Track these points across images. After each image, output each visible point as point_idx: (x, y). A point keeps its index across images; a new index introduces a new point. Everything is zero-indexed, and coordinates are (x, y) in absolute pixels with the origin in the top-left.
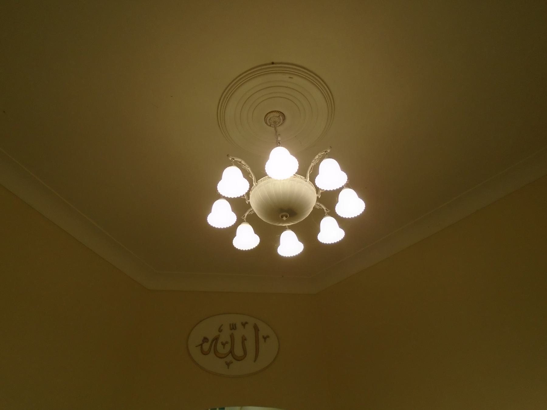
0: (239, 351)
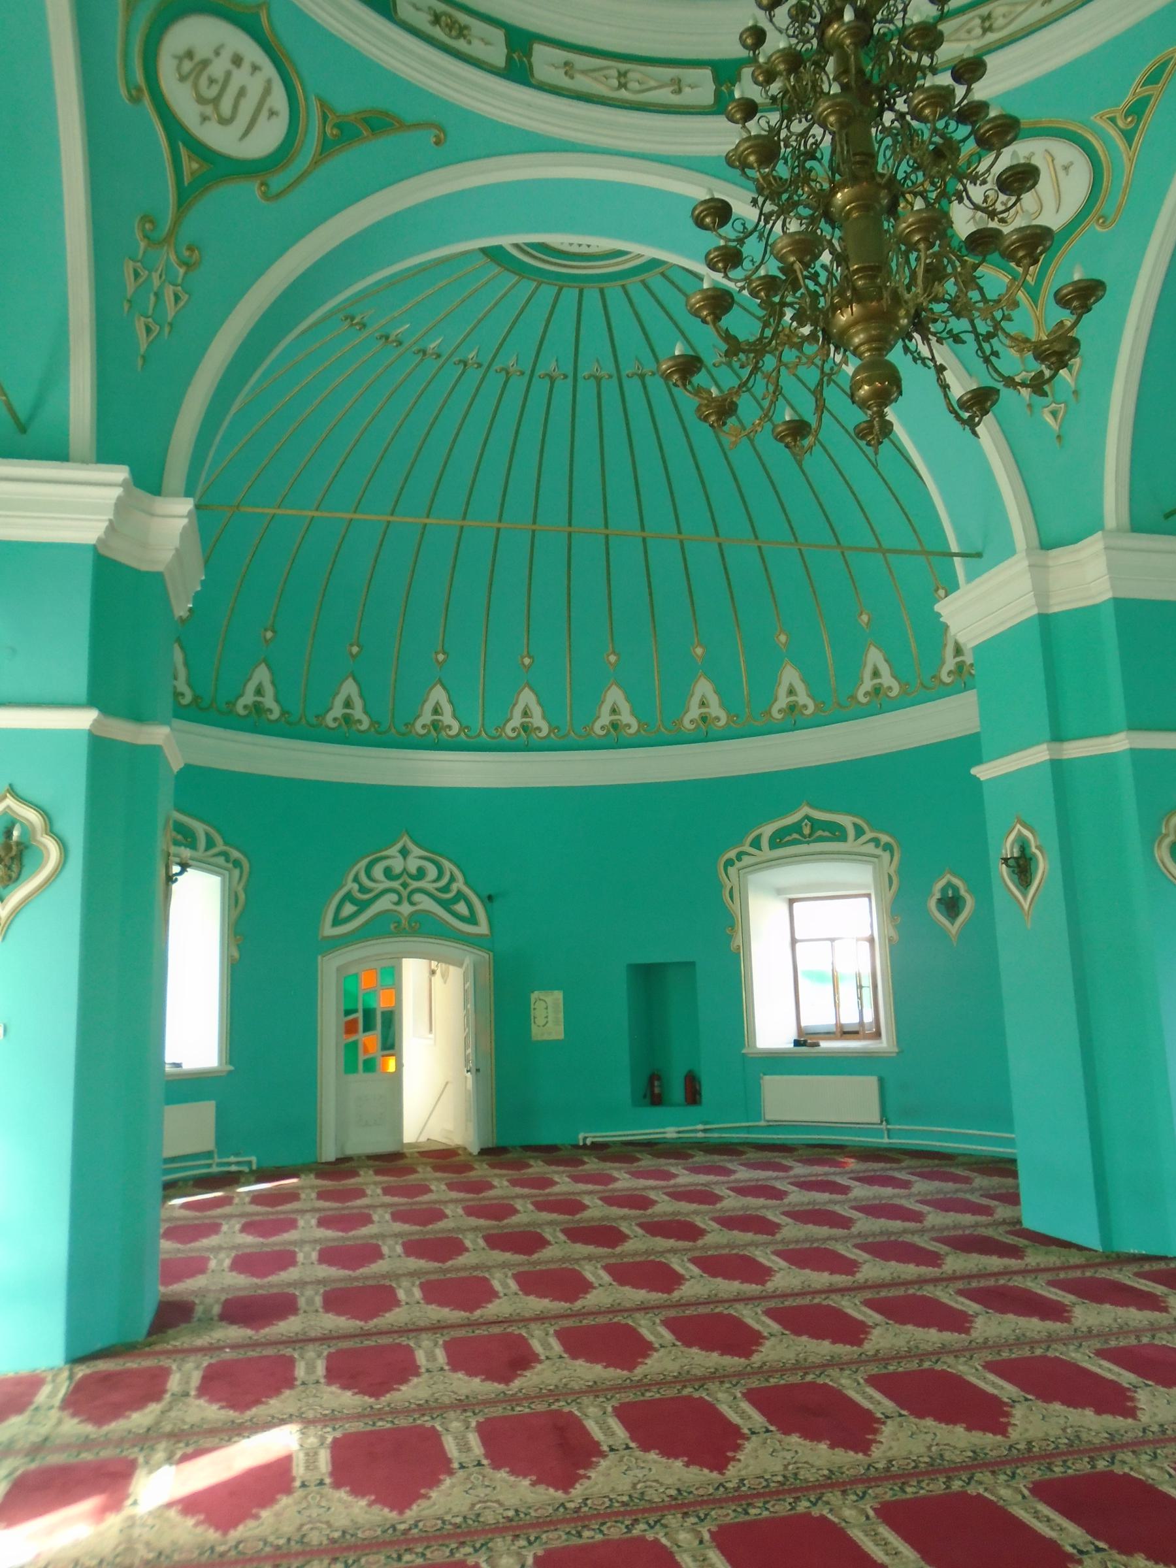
0: (226, 107)
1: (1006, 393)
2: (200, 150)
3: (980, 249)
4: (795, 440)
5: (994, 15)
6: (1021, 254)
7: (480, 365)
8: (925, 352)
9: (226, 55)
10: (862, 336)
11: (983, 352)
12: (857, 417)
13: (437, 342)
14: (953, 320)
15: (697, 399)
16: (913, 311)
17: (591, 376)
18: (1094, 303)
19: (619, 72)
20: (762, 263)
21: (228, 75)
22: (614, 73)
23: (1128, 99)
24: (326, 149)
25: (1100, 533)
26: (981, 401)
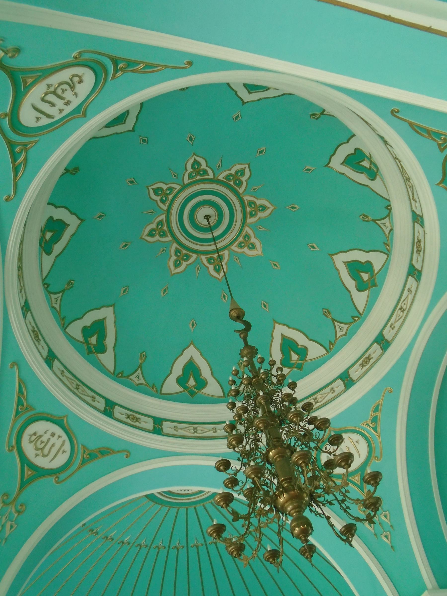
0: (46, 451)
1: (359, 525)
2: (33, 467)
3: (330, 467)
4: (274, 560)
5: (317, 398)
6: (343, 464)
7: (147, 546)
8: (320, 511)
9: (49, 433)
10: (291, 507)
11: (343, 508)
12: (299, 544)
13: (128, 538)
14: (326, 495)
15: (225, 544)
16: (309, 494)
17: (194, 545)
18: (380, 480)
19: (194, 428)
20: (246, 483)
21: (49, 439)
22: (192, 428)
23: (370, 417)
24: (84, 463)
25: (426, 591)
26: (349, 531)
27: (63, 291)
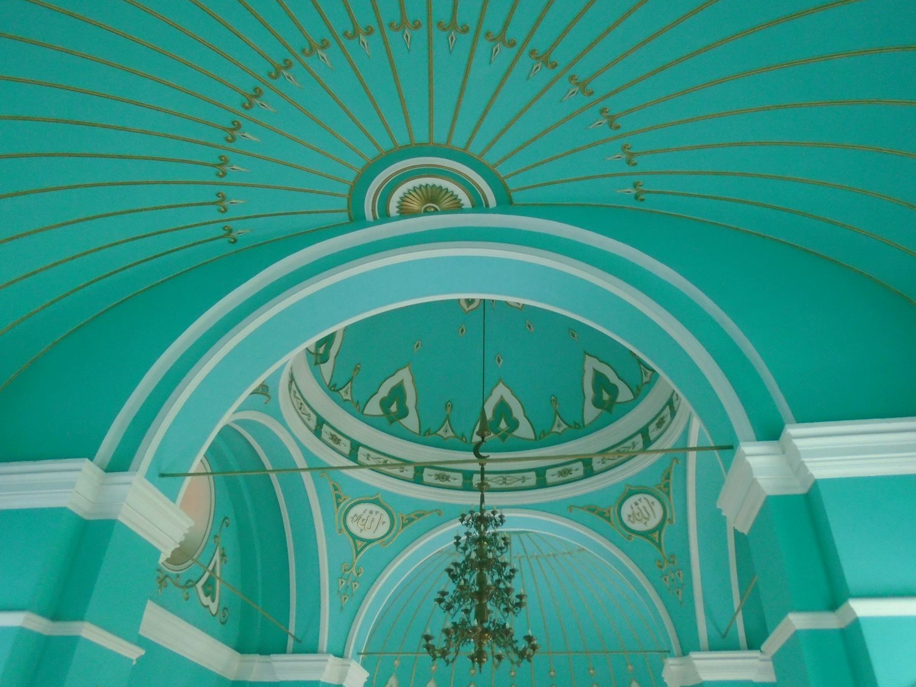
0: (646, 515)
2: (653, 531)
9: (634, 506)
27: (351, 380)
